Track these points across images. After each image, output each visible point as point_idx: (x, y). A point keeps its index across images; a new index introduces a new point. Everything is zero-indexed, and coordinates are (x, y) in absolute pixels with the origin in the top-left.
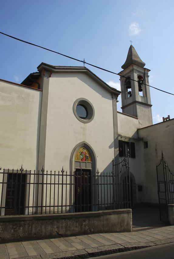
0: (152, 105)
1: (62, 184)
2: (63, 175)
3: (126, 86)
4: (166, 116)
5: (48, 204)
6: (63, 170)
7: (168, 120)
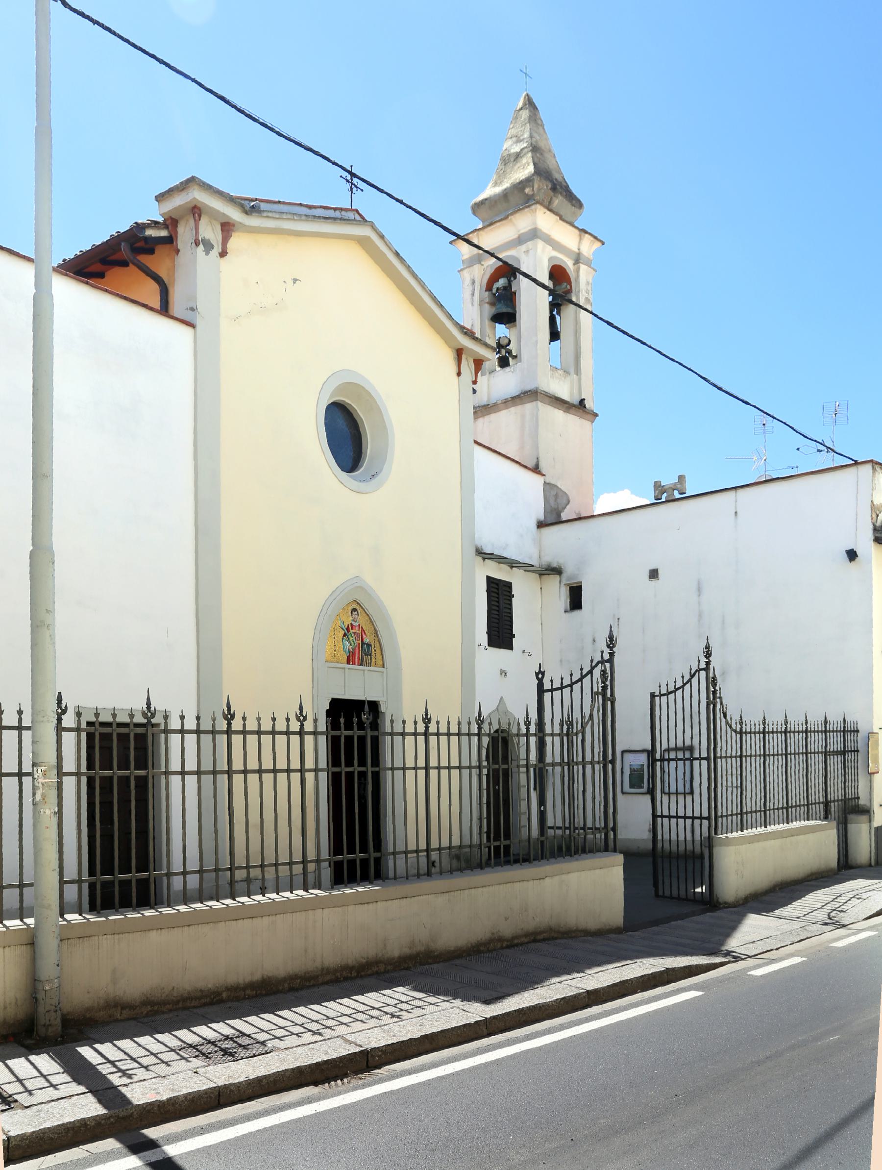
2: (229, 732)
4: (668, 480)
6: (527, 715)
7: (677, 495)
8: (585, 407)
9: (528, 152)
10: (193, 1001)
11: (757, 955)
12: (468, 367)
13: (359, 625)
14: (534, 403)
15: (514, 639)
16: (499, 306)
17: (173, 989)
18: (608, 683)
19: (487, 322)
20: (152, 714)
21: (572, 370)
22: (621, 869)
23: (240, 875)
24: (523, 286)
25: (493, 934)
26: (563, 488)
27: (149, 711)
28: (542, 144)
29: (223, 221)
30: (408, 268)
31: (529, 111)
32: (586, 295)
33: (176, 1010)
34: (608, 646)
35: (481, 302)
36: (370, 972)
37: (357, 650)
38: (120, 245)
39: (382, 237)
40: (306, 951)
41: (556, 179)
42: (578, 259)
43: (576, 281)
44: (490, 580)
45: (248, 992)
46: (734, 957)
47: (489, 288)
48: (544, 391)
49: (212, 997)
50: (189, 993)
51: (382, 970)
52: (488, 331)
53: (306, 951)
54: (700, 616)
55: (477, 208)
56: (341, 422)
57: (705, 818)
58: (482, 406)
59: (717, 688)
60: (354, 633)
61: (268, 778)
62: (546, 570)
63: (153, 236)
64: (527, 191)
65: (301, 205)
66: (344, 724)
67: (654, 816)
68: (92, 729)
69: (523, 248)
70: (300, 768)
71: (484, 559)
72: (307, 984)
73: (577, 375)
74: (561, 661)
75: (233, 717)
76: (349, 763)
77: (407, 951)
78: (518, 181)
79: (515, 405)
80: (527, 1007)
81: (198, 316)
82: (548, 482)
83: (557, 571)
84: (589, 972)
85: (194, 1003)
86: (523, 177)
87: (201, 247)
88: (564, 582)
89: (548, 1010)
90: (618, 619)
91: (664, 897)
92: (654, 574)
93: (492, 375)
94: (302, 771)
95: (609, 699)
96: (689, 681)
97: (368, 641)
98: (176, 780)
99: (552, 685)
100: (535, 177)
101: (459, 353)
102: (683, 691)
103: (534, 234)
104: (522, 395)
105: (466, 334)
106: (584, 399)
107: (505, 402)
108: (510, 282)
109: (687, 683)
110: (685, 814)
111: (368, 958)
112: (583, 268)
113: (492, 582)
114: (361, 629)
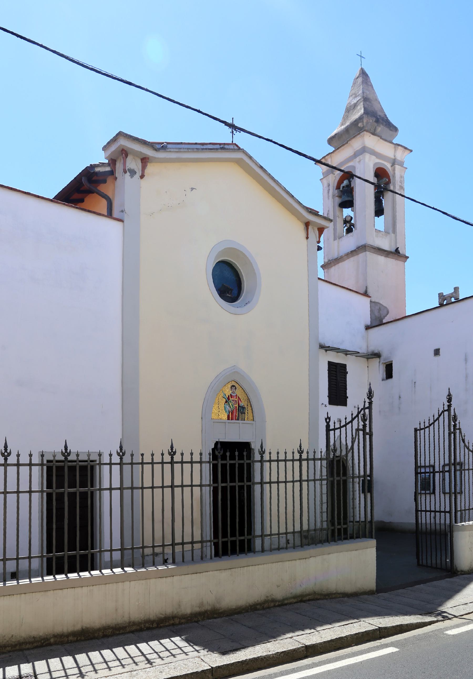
0: (407, 257)
1: (172, 487)
3: (338, 200)
4: (447, 291)
5: (275, 531)
6: (300, 447)
7: (453, 300)
8: (399, 253)
9: (361, 102)
10: (28, 645)
11: (463, 615)
12: (313, 233)
13: (236, 395)
14: (364, 253)
15: (347, 399)
16: (343, 197)
17: (12, 636)
18: (367, 422)
19: (337, 208)
20: (68, 453)
21: (391, 232)
22: (374, 550)
23: (148, 551)
24: (358, 184)
25: (267, 597)
26: (384, 304)
27: (172, 451)
28: (370, 96)
29: (142, 158)
30: (269, 175)
31: (362, 78)
32: (400, 184)
33: (14, 651)
34: (368, 398)
35: (333, 196)
36: (167, 624)
37: (235, 411)
38: (81, 179)
39: (250, 158)
40: (116, 610)
41: (380, 116)
42: (394, 162)
43: (393, 176)
44: (330, 364)
45: (71, 638)
46: (444, 617)
47: (338, 187)
48: (370, 245)
49: (43, 642)
50: (24, 639)
51: (177, 623)
52: (338, 213)
53: (116, 610)
54: (467, 377)
55: (331, 141)
56: (228, 273)
57: (447, 512)
58: (334, 259)
59: (457, 423)
60: (233, 400)
61: (282, 464)
62: (371, 355)
63: (101, 171)
64: (360, 125)
65: (196, 144)
66: (238, 456)
67: (417, 511)
68: (51, 464)
69: (357, 159)
70: (299, 479)
71: (326, 351)
72: (118, 633)
73: (394, 234)
74: (380, 411)
75: (175, 453)
76: (233, 480)
77: (197, 609)
78: (354, 120)
79: (353, 256)
80: (250, 659)
81: (125, 215)
82: (373, 301)
83: (377, 355)
84: (319, 628)
85: (28, 646)
86: (357, 117)
87: (128, 174)
88: (382, 362)
89: (268, 661)
90: (415, 382)
91: (422, 565)
92: (437, 352)
93: (341, 239)
94: (301, 481)
95: (367, 434)
96: (438, 419)
97: (242, 404)
98: (106, 494)
99: (334, 426)
100: (364, 116)
101: (307, 224)
102: (434, 426)
103: (364, 150)
104: (357, 249)
105: (310, 212)
106: (398, 248)
107: (347, 255)
108: (350, 182)
109: (436, 420)
110: (430, 509)
111: (166, 614)
112: (397, 167)
113: (332, 365)
114: (237, 398)
